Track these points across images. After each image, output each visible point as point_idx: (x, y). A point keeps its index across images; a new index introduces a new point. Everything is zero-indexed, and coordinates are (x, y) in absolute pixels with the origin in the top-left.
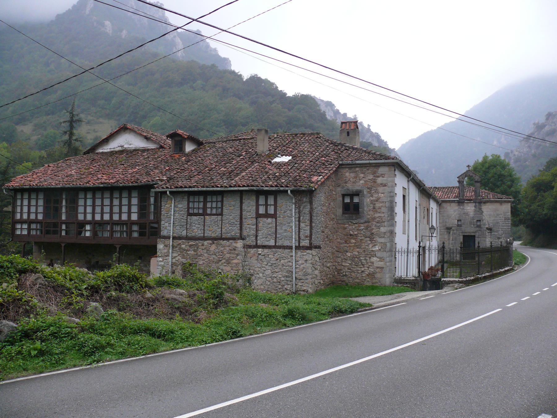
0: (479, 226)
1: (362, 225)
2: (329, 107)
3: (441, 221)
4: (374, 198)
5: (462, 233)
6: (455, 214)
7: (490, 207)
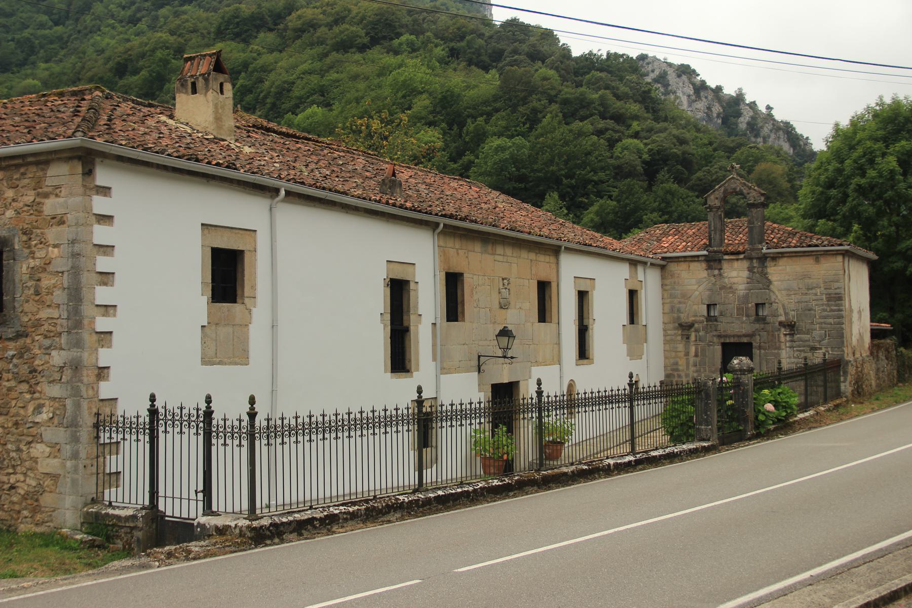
1: (12, 344)
2: (684, 77)
4: (37, 262)
5: (719, 336)
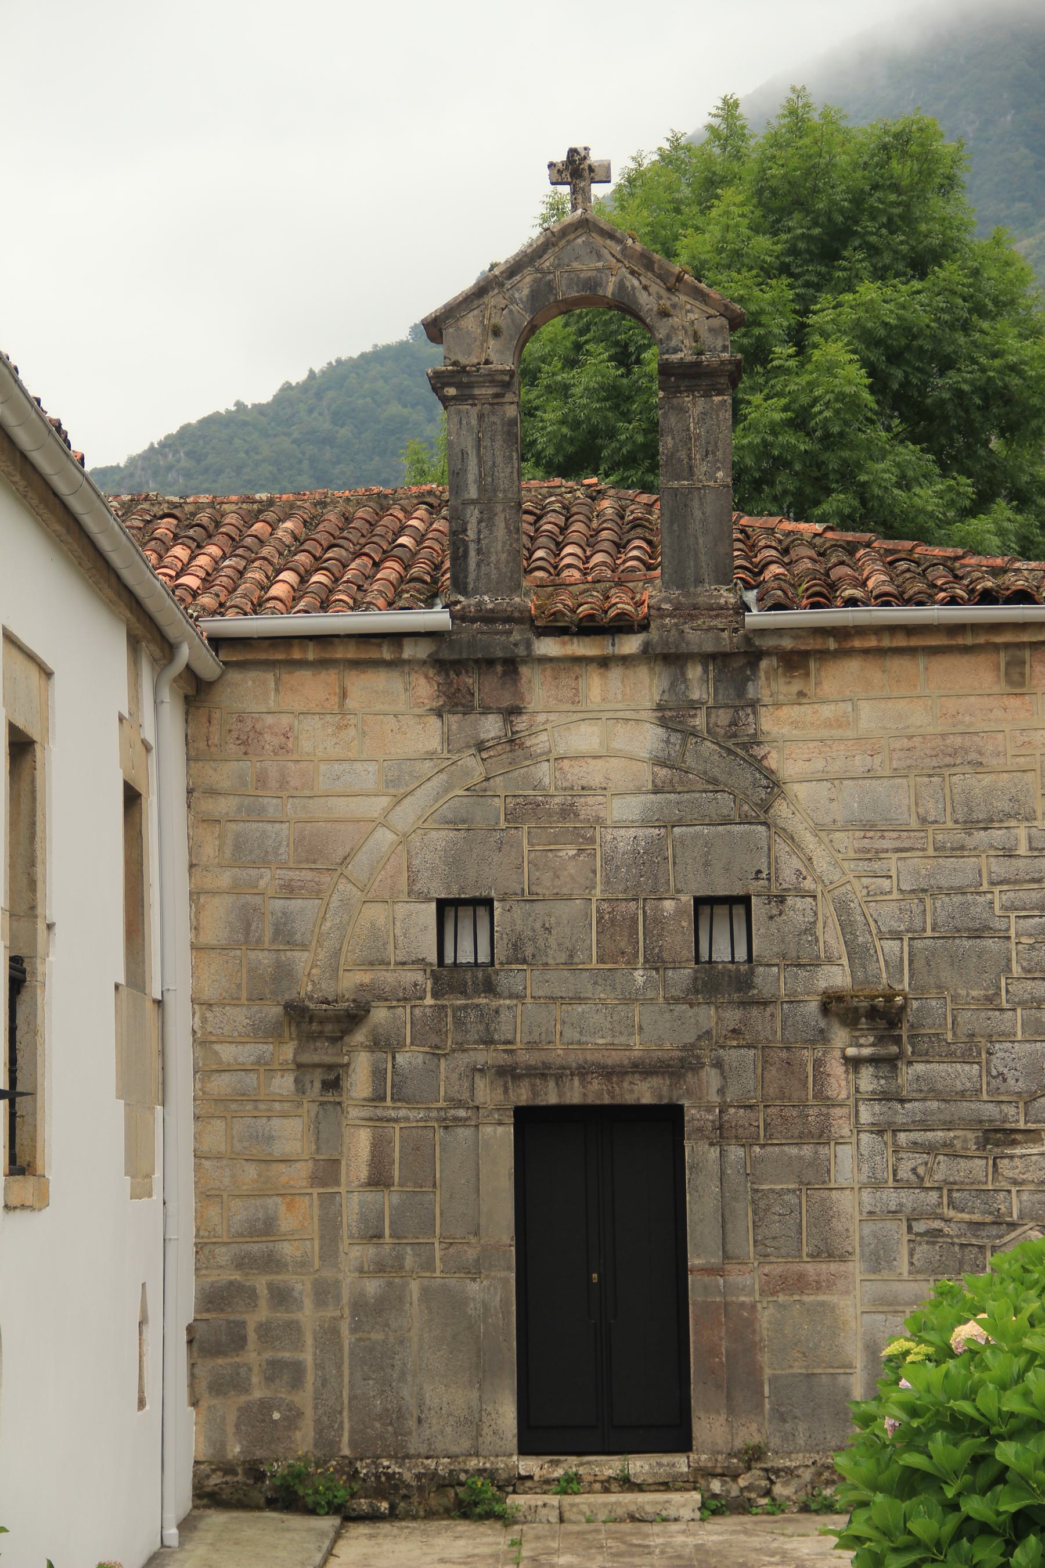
0: (726, 985)
3: (218, 912)
5: (508, 1073)
6: (407, 814)
7: (869, 716)
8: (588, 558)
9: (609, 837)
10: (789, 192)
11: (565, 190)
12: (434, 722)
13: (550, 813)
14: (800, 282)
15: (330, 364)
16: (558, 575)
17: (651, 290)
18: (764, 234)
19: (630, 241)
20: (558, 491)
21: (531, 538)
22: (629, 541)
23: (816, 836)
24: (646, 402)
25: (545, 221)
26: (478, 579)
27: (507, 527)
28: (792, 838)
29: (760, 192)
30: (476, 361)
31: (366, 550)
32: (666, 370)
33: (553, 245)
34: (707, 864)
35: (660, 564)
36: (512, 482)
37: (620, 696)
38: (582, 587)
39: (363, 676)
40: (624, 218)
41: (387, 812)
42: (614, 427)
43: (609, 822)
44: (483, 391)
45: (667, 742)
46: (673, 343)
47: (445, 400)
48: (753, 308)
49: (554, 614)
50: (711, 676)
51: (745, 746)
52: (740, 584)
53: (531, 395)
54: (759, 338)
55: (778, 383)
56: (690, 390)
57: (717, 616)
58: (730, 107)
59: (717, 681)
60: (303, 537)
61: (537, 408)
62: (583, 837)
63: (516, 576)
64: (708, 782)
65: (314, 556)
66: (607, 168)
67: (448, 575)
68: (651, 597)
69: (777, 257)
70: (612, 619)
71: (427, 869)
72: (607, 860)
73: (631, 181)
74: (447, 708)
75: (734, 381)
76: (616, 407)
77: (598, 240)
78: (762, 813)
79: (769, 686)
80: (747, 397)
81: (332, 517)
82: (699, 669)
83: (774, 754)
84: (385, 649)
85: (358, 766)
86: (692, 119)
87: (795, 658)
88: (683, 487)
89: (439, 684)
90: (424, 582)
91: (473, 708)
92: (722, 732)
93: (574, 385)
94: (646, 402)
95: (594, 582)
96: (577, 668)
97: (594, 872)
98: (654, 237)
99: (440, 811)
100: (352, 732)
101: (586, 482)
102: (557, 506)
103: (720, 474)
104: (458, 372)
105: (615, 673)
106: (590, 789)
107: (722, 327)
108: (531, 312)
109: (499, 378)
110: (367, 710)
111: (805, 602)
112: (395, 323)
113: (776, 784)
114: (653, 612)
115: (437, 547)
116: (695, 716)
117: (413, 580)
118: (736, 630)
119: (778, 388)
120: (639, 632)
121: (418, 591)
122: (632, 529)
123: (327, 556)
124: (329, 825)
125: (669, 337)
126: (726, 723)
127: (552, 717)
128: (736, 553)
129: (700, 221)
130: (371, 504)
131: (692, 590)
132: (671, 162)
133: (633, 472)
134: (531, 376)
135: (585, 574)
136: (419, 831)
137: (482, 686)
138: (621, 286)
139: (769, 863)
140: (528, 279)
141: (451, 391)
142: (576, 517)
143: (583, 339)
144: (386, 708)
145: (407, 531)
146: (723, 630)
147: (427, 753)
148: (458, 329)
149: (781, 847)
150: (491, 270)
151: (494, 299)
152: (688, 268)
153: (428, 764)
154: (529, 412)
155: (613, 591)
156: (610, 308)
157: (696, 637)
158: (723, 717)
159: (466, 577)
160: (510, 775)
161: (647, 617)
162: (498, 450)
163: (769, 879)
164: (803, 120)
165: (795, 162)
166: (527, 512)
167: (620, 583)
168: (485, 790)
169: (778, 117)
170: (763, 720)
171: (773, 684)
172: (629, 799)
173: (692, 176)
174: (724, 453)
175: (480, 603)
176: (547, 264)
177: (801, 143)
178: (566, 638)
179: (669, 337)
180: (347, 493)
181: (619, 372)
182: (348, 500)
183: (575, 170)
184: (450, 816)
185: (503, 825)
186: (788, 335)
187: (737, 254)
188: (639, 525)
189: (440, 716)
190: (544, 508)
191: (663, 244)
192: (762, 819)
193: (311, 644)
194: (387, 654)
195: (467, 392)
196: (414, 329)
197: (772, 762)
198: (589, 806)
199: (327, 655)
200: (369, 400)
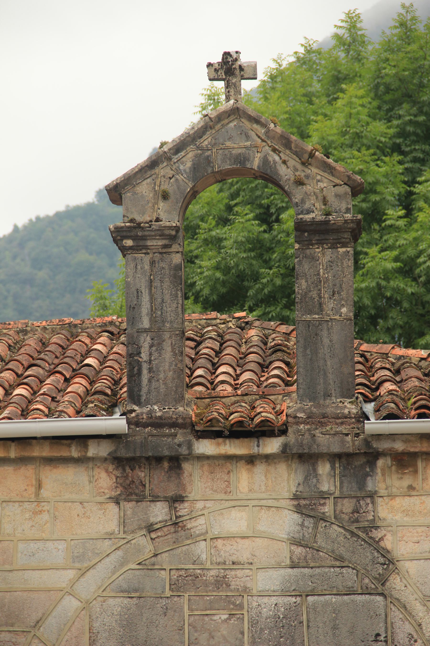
8: (238, 376)
9: (255, 604)
10: (400, 87)
11: (221, 84)
12: (112, 508)
13: (206, 584)
14: (408, 158)
15: (31, 220)
16: (214, 389)
17: (288, 163)
18: (380, 120)
19: (272, 126)
20: (214, 322)
21: (192, 359)
22: (271, 363)
23: (425, 605)
24: (284, 253)
25: (204, 109)
26: (149, 392)
27: (173, 350)
28: (405, 607)
29: (377, 86)
30: (148, 219)
31: (59, 369)
32: (300, 227)
33: (211, 128)
34: (335, 628)
35: (296, 381)
36: (177, 315)
37: (263, 488)
38: (233, 399)
39: (55, 470)
40: (267, 107)
41: (73, 583)
42: (258, 272)
43: (254, 592)
44: (154, 243)
45: (302, 525)
46: (307, 206)
47: (124, 250)
48: (370, 179)
49: (210, 420)
50: (337, 472)
51: (365, 530)
52: (361, 398)
53: (193, 246)
54: (375, 204)
55: (390, 239)
56: (320, 243)
57: (342, 423)
58: (352, 22)
59: (342, 476)
60: (7, 359)
61: (197, 257)
62: (234, 604)
63: (180, 390)
64: (336, 559)
65: (17, 374)
66: (254, 68)
67: (125, 389)
68: (288, 407)
69: (390, 138)
70: (258, 425)
71: (105, 631)
72: (253, 623)
73: (273, 78)
74: (123, 497)
75: (355, 238)
76: (261, 256)
77: (247, 124)
78: (379, 586)
79: (385, 481)
80: (365, 250)
81: (32, 342)
82: (328, 466)
83: (389, 537)
84: (73, 448)
85: (49, 544)
86: (321, 29)
87: (406, 458)
88: (314, 320)
89: (117, 477)
90: (106, 394)
91: (144, 497)
92: (347, 518)
93: (226, 239)
94: (284, 253)
95: (242, 395)
96: (228, 465)
97: (242, 633)
98: (291, 122)
99: (117, 582)
100: (45, 517)
101: (237, 315)
102: (213, 334)
103: (344, 310)
104: (134, 227)
105: (260, 469)
106: (239, 563)
107: (346, 193)
108: (193, 181)
109: (167, 232)
110: (58, 498)
111: (413, 413)
112: (84, 187)
113: (391, 562)
114: (290, 420)
115: (116, 366)
116: (324, 504)
117: (97, 392)
118: (357, 435)
119: (390, 242)
120: (279, 436)
121: (101, 402)
122: (273, 353)
123: (27, 373)
124: (25, 594)
125: (303, 201)
126: (350, 510)
127: (209, 504)
128: (357, 373)
129: (328, 110)
130: (63, 332)
131: (322, 402)
132: (305, 63)
133: (273, 308)
134: (191, 230)
135: (236, 389)
136: (100, 599)
137: (155, 479)
138: (265, 161)
139: (386, 628)
140: (191, 155)
141: (129, 243)
142: (228, 343)
143: (233, 203)
144: (74, 497)
145: (93, 354)
146: (347, 435)
147: (107, 533)
148: (135, 193)
149: (396, 614)
150: (161, 147)
151: (163, 170)
152: (319, 147)
153: (107, 543)
154: (191, 260)
155: (258, 402)
156: (256, 178)
157: (326, 441)
158: (347, 506)
159: (140, 390)
160: (174, 552)
161: (286, 424)
162: (166, 290)
163: (386, 641)
164: (411, 30)
165: (404, 63)
166: (189, 339)
167: (263, 396)
168: (154, 565)
169: (391, 28)
170: (380, 509)
171: (388, 481)
172: (271, 572)
173: (324, 73)
174: (348, 293)
175: (151, 412)
176: (206, 143)
177: (409, 48)
178: (220, 440)
179: (303, 201)
180: (44, 323)
181: (262, 229)
182: (45, 328)
183: (229, 69)
184: (125, 586)
185: (168, 593)
186: (399, 200)
187: (358, 136)
188: (279, 350)
189: (118, 503)
190: (203, 335)
191: (298, 128)
192: (380, 590)
193: (13, 444)
194: (75, 452)
195: (141, 243)
196: (99, 193)
197: (388, 543)
198: (238, 578)
199: (26, 454)
200: (62, 249)
